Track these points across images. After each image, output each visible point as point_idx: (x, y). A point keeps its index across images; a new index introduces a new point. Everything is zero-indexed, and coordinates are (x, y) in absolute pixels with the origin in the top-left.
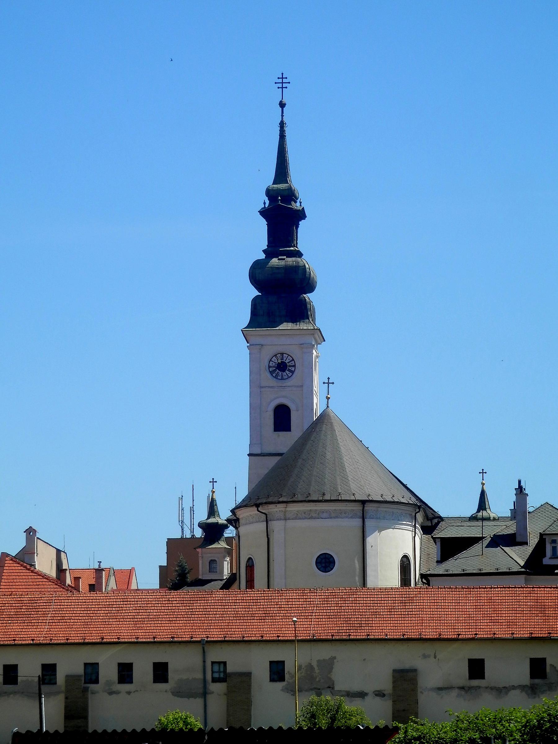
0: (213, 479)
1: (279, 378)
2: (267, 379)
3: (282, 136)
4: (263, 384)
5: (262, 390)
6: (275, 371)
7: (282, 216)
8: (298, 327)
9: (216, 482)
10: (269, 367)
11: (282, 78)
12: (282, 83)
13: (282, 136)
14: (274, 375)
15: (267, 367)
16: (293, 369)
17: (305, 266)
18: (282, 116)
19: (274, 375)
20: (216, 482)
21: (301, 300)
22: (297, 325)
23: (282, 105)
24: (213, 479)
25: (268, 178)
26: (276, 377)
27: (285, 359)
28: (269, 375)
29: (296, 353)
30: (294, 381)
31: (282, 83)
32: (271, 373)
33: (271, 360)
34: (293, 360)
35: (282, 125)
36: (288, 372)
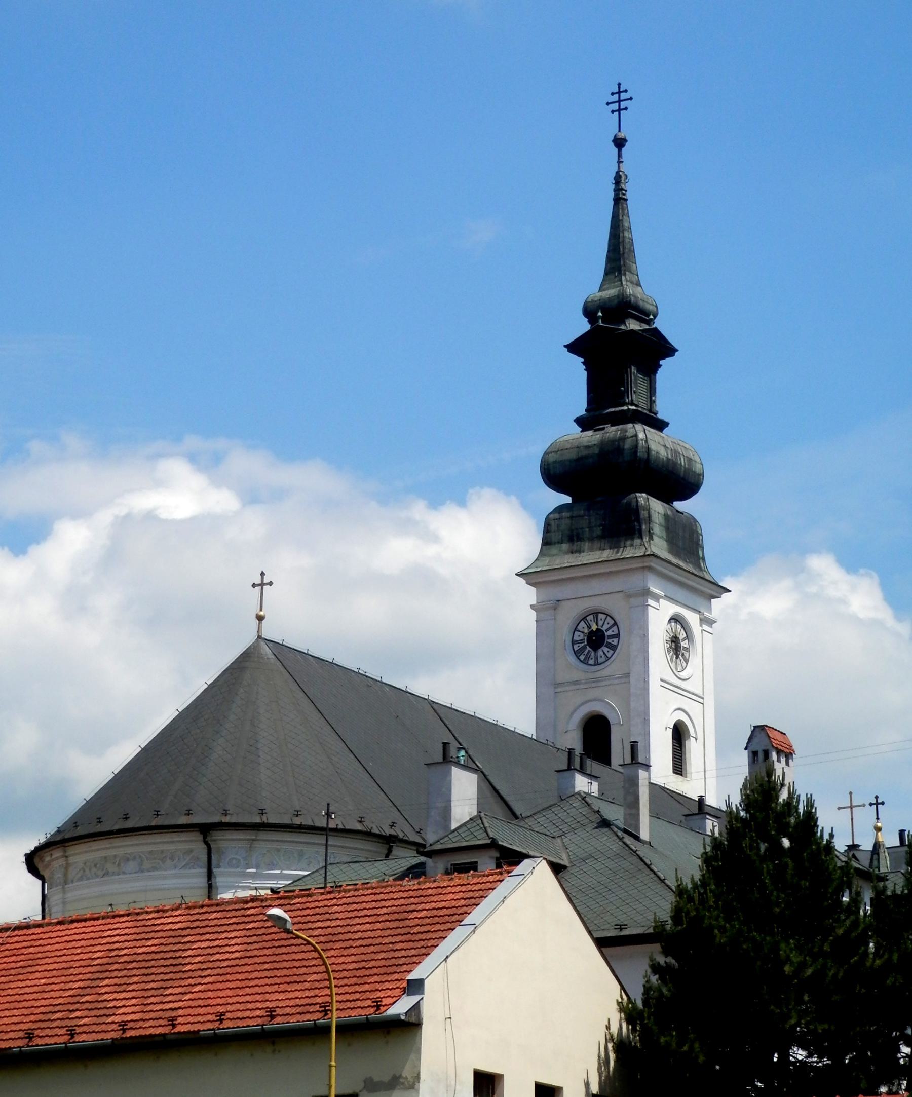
0: (877, 797)
1: (591, 662)
2: (569, 666)
3: (619, 200)
4: (560, 679)
5: (559, 690)
6: (582, 650)
7: (620, 348)
8: (619, 556)
9: (883, 803)
10: (574, 642)
11: (619, 92)
12: (619, 101)
13: (619, 200)
14: (582, 657)
15: (569, 643)
16: (615, 641)
17: (636, 436)
18: (619, 162)
19: (582, 657)
20: (883, 803)
21: (629, 504)
22: (617, 552)
23: (620, 143)
24: (877, 797)
25: (589, 281)
26: (585, 662)
27: (600, 623)
28: (572, 659)
29: (616, 606)
30: (612, 668)
31: (619, 101)
32: (577, 654)
33: (576, 630)
34: (615, 624)
35: (618, 179)
36: (606, 649)
